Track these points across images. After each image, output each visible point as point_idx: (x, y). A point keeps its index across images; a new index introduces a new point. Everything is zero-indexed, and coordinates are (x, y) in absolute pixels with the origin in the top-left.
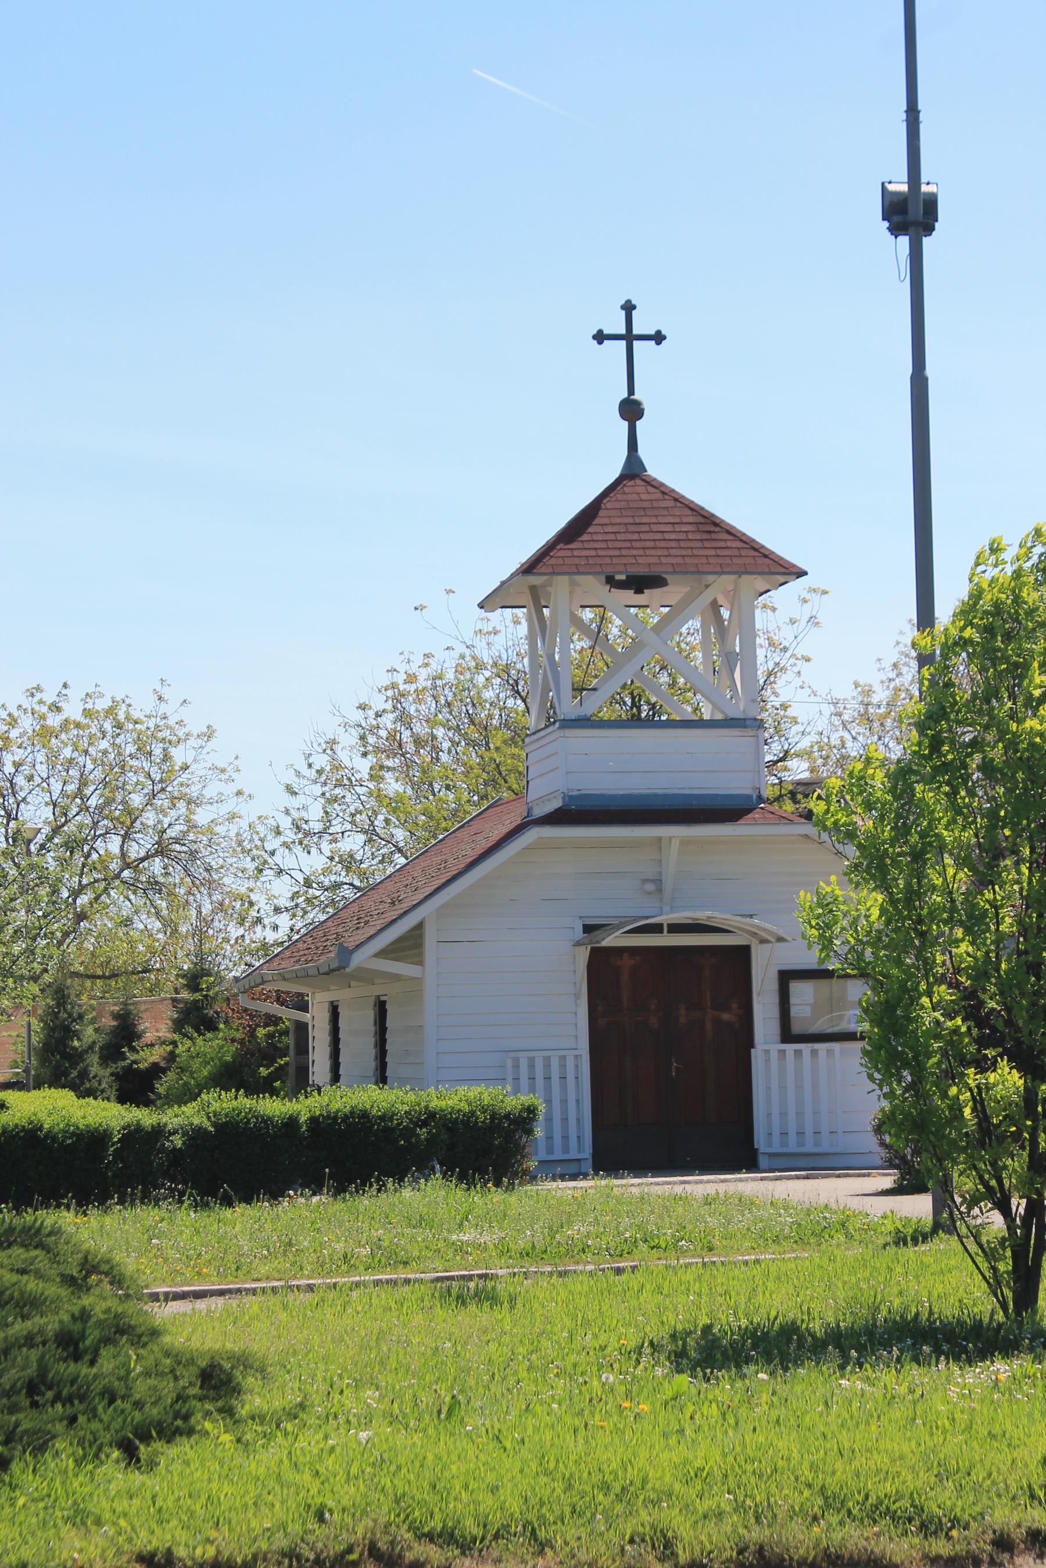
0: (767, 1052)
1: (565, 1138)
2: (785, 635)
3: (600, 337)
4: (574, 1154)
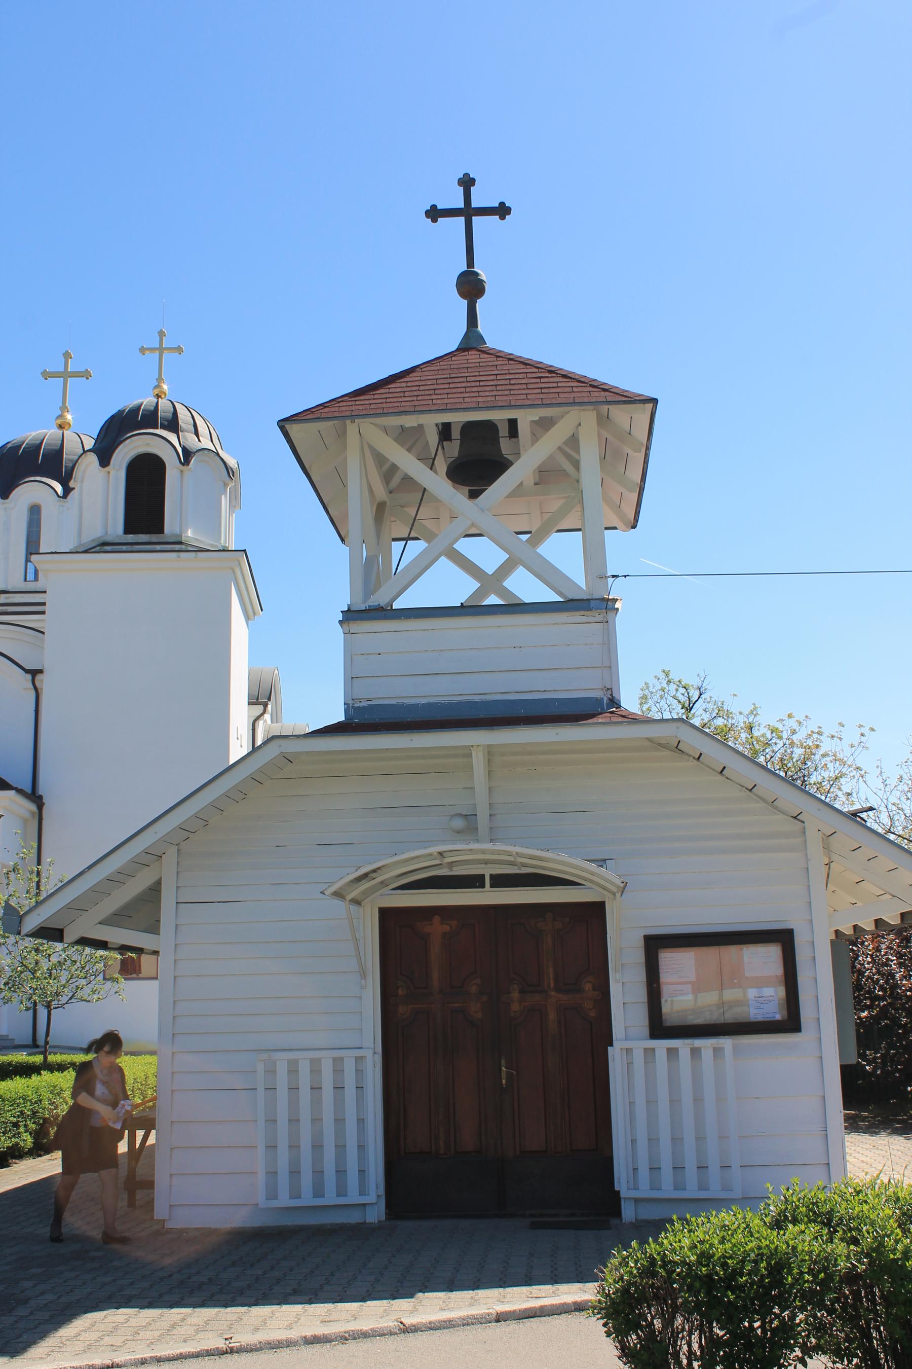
0: (629, 1051)
1: (341, 1172)
2: (845, 753)
3: (434, 214)
4: (353, 1197)
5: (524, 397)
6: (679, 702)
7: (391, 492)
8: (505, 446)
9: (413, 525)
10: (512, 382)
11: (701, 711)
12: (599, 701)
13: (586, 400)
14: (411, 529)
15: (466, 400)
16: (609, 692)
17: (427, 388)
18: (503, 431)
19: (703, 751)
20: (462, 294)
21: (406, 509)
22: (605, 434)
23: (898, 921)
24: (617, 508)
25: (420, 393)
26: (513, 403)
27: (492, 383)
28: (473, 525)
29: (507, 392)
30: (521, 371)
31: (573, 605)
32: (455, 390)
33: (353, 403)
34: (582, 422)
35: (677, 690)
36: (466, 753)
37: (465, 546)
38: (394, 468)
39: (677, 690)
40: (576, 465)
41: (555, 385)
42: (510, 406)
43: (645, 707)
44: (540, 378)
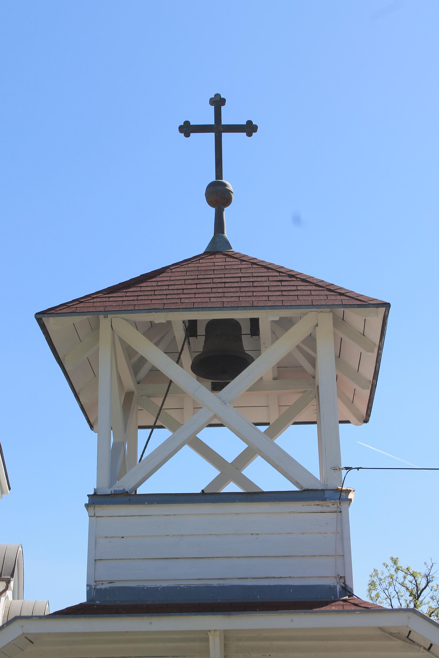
3: (187, 129)
5: (266, 298)
6: (407, 589)
7: (138, 383)
8: (247, 343)
9: (158, 415)
10: (255, 284)
11: (428, 599)
12: (332, 589)
13: (323, 303)
14: (157, 418)
15: (212, 300)
16: (342, 580)
17: (176, 287)
18: (246, 329)
19: (434, 641)
20: (211, 203)
21: (151, 399)
22: (341, 334)
23: (349, 498)
24: (350, 404)
25: (170, 292)
26: (255, 304)
27: (236, 285)
28: (215, 416)
29: (250, 294)
30: (264, 275)
31: (307, 494)
32: (202, 291)
33: (107, 299)
34: (319, 323)
35: (405, 578)
36: (203, 637)
37: (207, 436)
38: (142, 360)
39: (405, 578)
40: (313, 362)
41: (294, 288)
42: (253, 307)
43: (374, 594)
44: (281, 281)
